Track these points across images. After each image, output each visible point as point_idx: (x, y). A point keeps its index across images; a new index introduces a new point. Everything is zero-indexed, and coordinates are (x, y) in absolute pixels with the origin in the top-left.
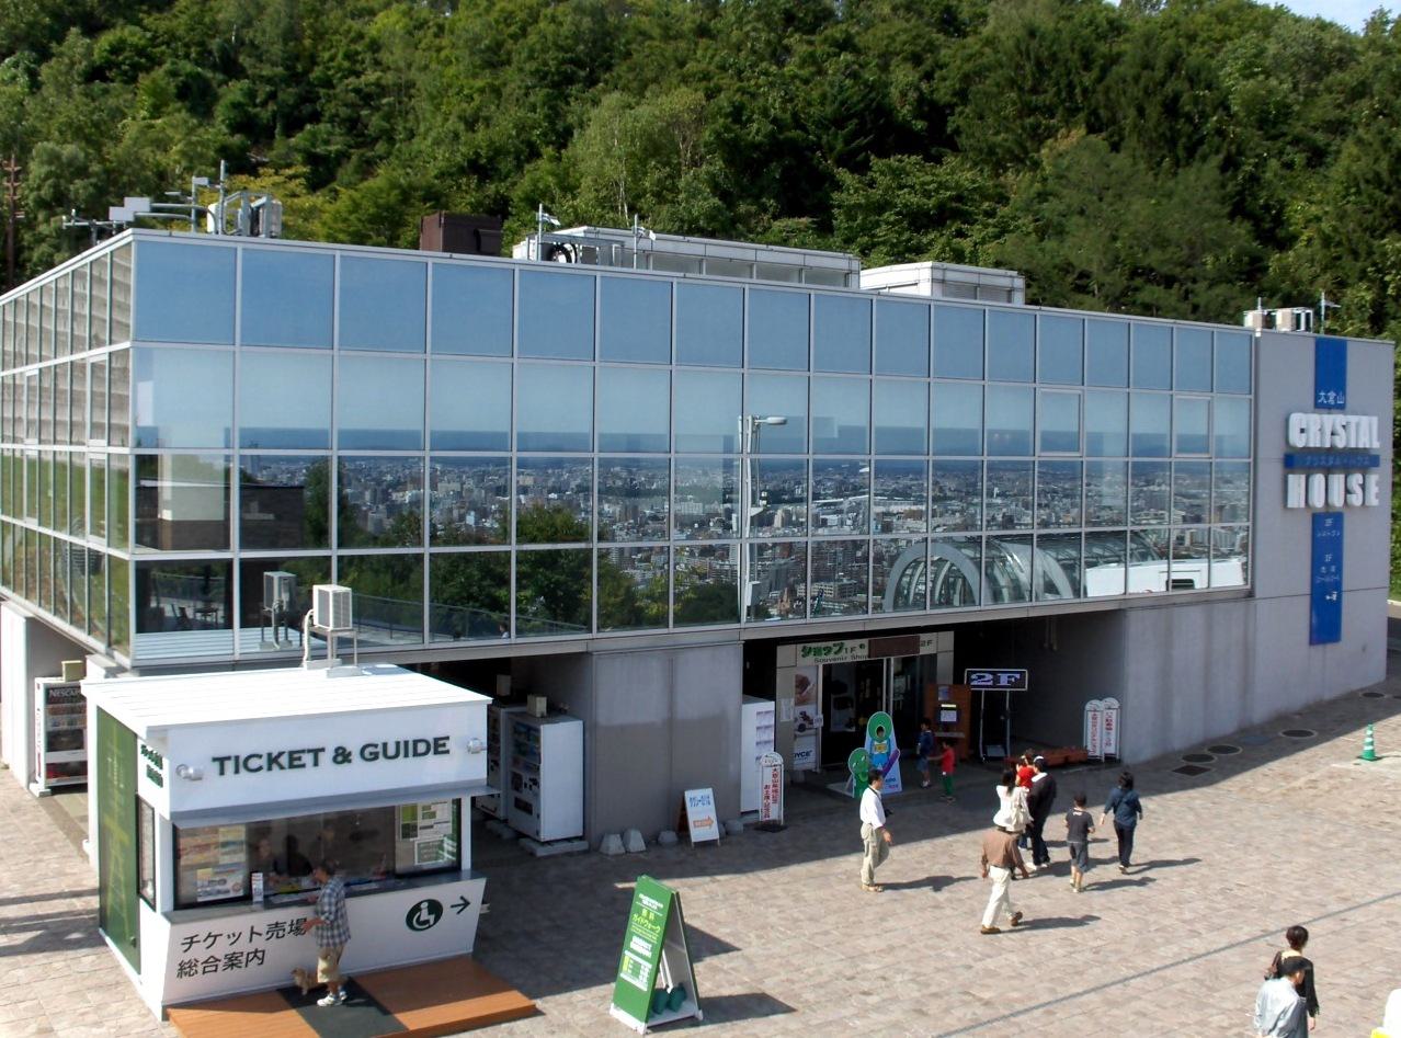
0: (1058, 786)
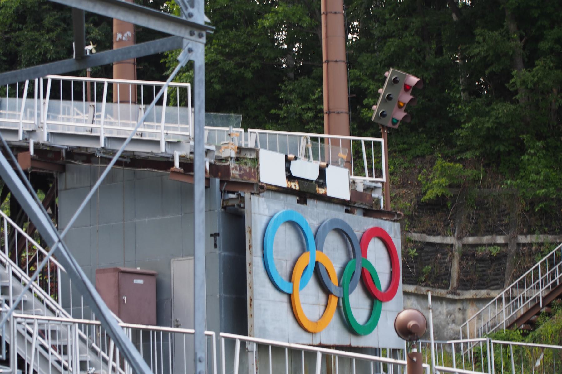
0: (118, 267)
